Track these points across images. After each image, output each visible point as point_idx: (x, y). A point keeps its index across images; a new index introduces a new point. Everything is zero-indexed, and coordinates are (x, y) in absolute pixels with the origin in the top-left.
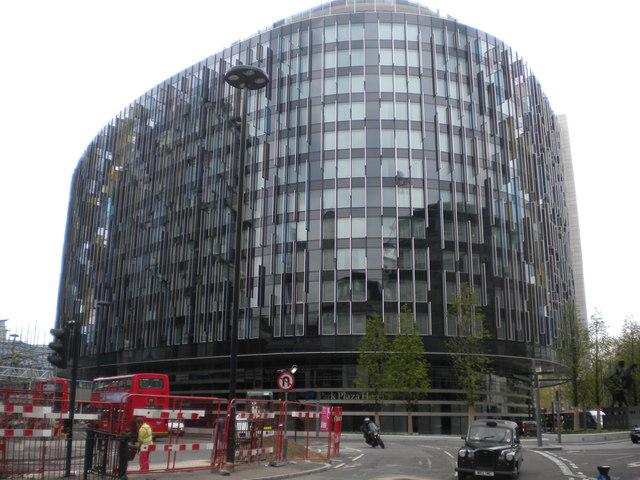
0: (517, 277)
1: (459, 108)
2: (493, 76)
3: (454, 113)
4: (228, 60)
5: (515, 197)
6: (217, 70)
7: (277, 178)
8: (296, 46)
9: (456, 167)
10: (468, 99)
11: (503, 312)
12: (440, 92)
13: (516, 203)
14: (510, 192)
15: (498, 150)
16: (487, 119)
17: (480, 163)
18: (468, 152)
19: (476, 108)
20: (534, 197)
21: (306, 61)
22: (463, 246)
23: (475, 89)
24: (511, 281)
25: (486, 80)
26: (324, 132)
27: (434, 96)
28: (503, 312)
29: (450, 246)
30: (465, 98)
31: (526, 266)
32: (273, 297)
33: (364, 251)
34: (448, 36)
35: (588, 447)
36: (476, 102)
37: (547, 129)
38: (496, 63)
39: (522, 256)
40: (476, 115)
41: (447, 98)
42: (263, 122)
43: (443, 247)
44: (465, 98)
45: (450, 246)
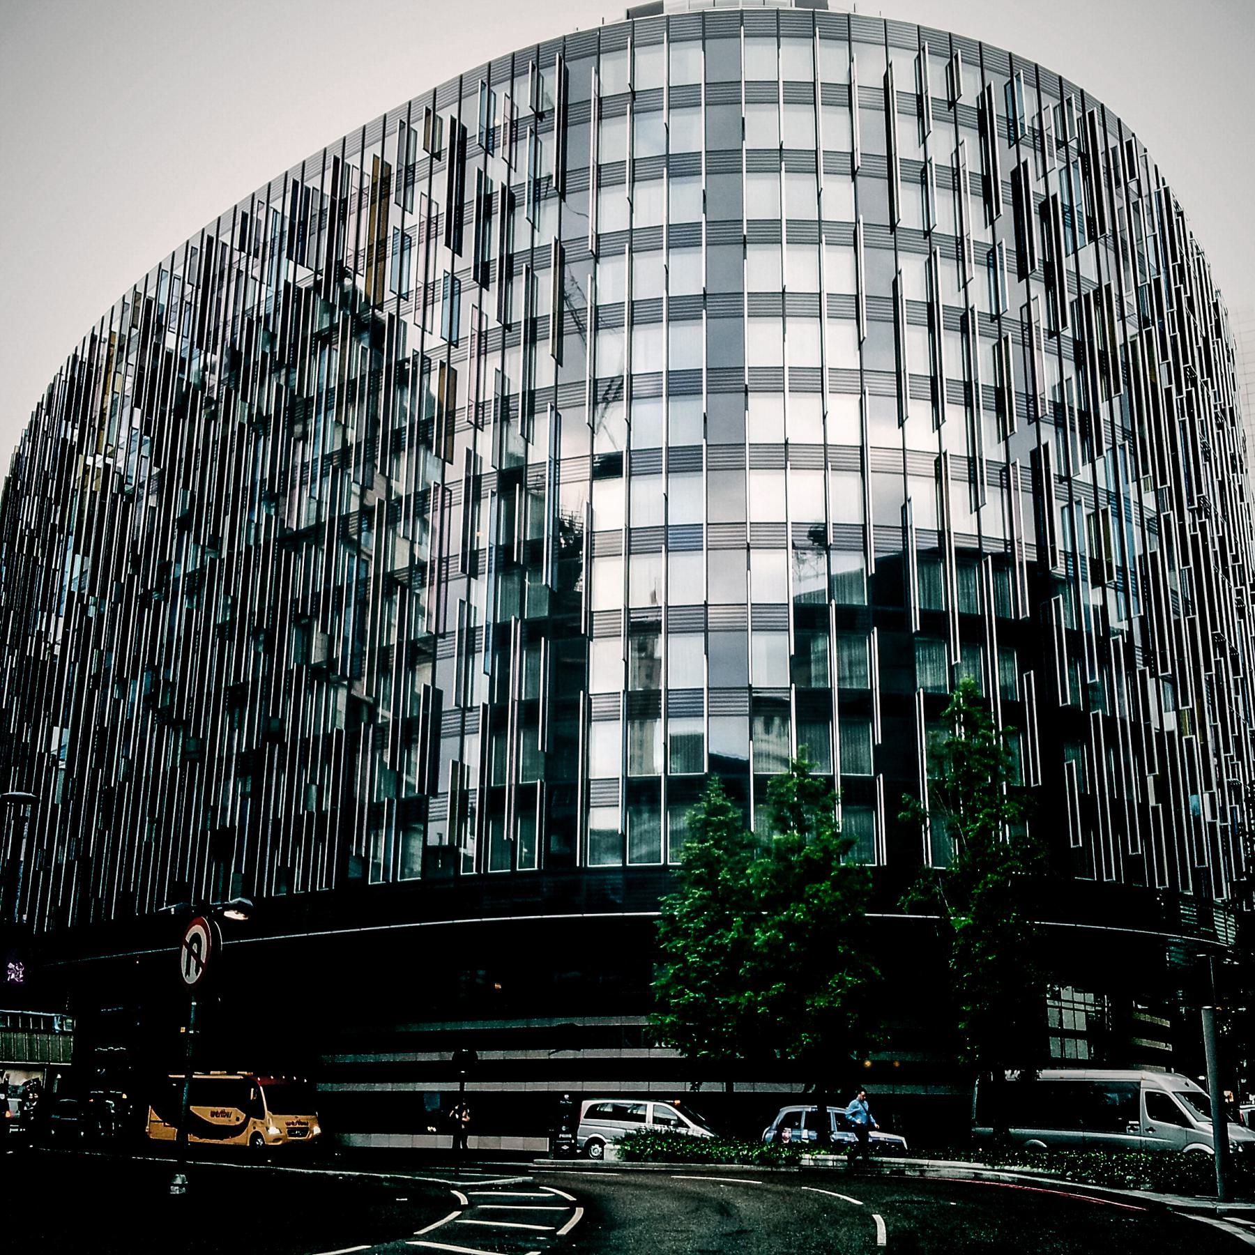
0: (1124, 708)
1: (960, 258)
2: (1053, 178)
3: (946, 271)
4: (354, 161)
5: (1115, 497)
6: (328, 191)
7: (472, 457)
8: (525, 109)
9: (955, 415)
10: (986, 237)
11: (1088, 802)
12: (909, 217)
13: (1118, 515)
14: (1101, 484)
15: (1070, 370)
16: (1038, 289)
17: (1017, 405)
18: (985, 376)
19: (1008, 261)
20: (1172, 498)
21: (550, 144)
22: (973, 628)
23: (1007, 211)
24: (1110, 722)
25: (1036, 187)
26: (596, 329)
27: (893, 227)
28: (1088, 802)
29: (935, 622)
30: (977, 232)
31: (1151, 683)
32: (459, 768)
33: (700, 638)
34: (935, 71)
35: (1074, 1184)
36: (1008, 242)
37: (1201, 332)
38: (1062, 144)
39: (1139, 655)
40: (1008, 279)
41: (927, 233)
42: (439, 313)
43: (916, 626)
44: (977, 232)
45: (935, 622)
